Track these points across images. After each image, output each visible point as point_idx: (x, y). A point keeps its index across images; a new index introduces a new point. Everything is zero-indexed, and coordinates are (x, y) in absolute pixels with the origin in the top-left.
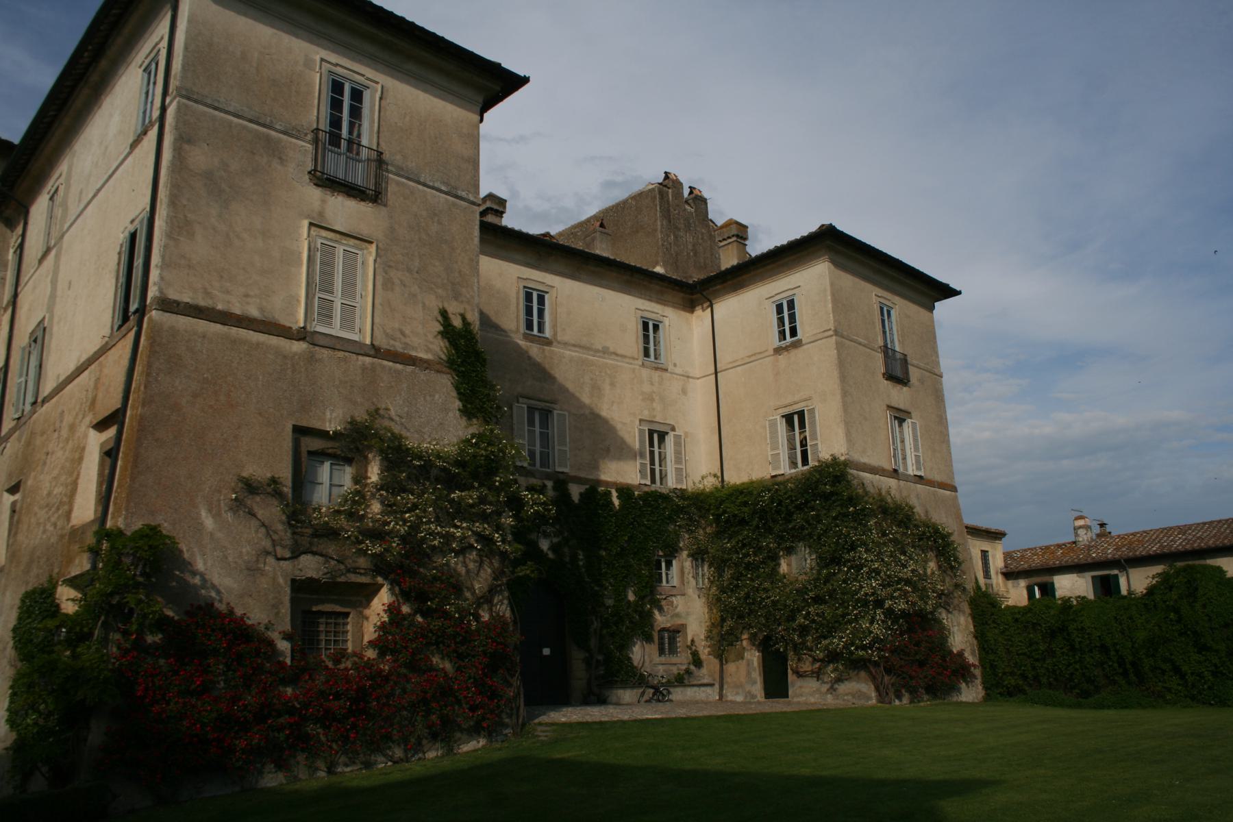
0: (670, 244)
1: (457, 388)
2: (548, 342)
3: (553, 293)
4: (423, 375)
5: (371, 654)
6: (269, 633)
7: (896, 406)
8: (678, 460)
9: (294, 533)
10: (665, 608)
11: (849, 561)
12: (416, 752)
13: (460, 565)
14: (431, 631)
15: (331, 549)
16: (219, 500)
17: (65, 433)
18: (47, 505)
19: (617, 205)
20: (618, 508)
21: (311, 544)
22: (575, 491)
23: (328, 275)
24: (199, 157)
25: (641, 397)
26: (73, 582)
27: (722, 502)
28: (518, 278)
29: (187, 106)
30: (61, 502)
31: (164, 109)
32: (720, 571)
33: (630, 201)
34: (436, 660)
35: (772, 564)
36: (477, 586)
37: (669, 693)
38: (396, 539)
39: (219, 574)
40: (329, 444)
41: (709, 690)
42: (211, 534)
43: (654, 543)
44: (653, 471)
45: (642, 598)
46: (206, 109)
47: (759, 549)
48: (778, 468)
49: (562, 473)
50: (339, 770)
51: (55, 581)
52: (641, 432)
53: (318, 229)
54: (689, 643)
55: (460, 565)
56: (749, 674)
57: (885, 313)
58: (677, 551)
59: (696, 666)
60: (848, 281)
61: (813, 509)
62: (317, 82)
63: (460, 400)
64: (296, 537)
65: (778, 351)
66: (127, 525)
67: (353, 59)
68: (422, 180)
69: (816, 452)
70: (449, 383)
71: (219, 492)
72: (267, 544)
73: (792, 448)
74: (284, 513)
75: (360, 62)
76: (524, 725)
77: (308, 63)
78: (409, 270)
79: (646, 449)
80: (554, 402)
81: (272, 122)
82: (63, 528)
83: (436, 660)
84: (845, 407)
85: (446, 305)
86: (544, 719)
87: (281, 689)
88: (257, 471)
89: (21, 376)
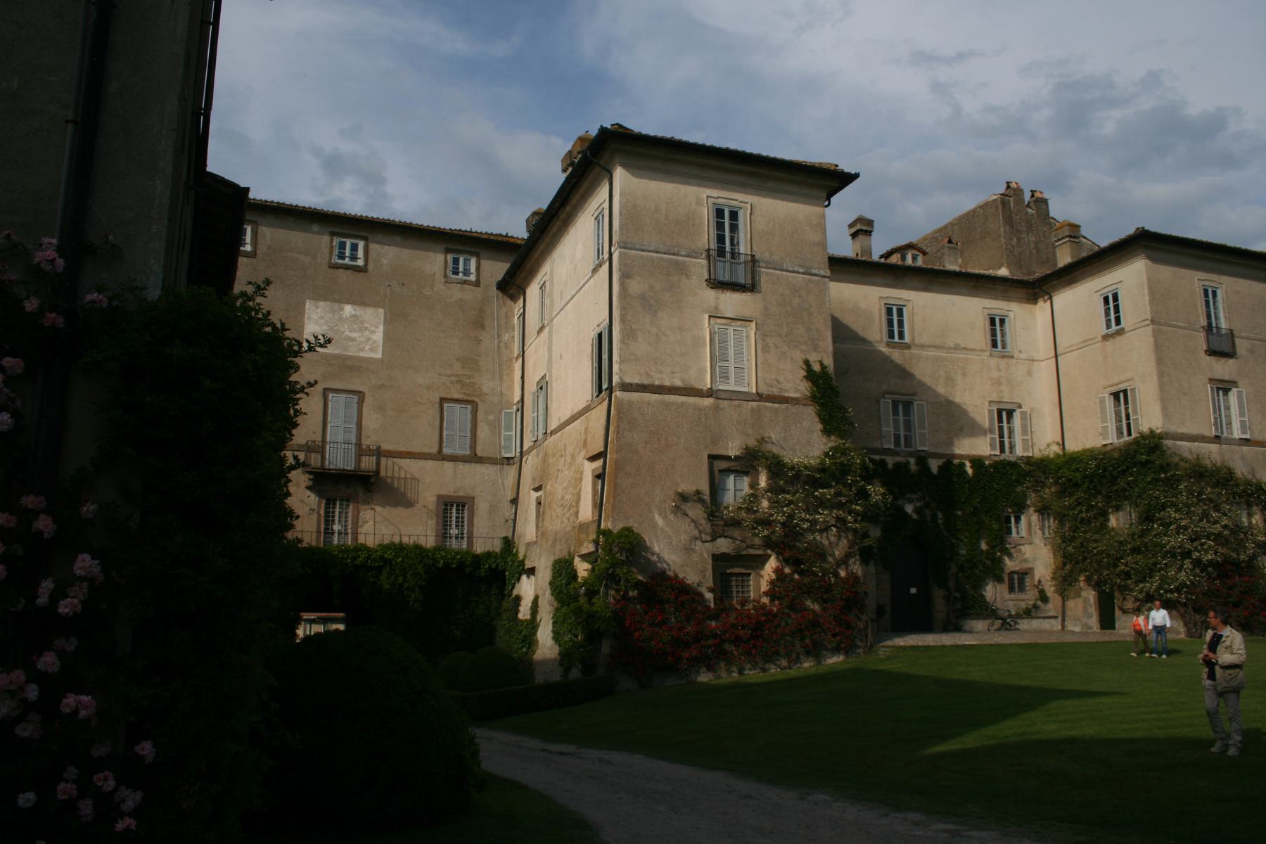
0: (1013, 246)
1: (819, 415)
2: (908, 347)
3: (910, 306)
4: (794, 409)
5: (765, 600)
6: (700, 588)
7: (1221, 378)
8: (1024, 432)
9: (712, 525)
10: (1015, 555)
11: (1160, 519)
12: (796, 664)
13: (824, 539)
14: (804, 584)
15: (737, 533)
16: (665, 508)
17: (568, 459)
18: (562, 506)
19: (969, 213)
20: (971, 475)
21: (723, 531)
22: (934, 465)
23: (724, 349)
24: (635, 286)
25: (989, 383)
26: (584, 557)
27: (1060, 469)
28: (880, 297)
29: (625, 253)
30: (571, 505)
31: (611, 255)
32: (1061, 523)
33: (978, 210)
34: (809, 603)
35: (1101, 519)
36: (837, 553)
37: (1016, 623)
38: (778, 525)
39: (668, 553)
40: (732, 464)
41: (1053, 621)
42: (662, 529)
43: (1003, 502)
44: (1002, 444)
45: (993, 547)
46: (636, 252)
47: (1090, 508)
48: (1108, 438)
49: (923, 451)
50: (746, 672)
51: (572, 556)
52: (990, 412)
53: (714, 319)
54: (1036, 583)
55: (824, 539)
56: (1085, 610)
57: (1209, 295)
58: (1024, 508)
59: (1042, 602)
60: (1167, 273)
61: (1132, 475)
62: (705, 215)
63: (822, 423)
64: (714, 527)
65: (1106, 337)
66: (614, 527)
67: (729, 190)
68: (785, 268)
69: (1137, 425)
70: (813, 412)
71: (665, 502)
72: (696, 533)
73: (1118, 419)
74: (705, 512)
75: (734, 191)
76: (871, 647)
77: (699, 203)
78: (780, 336)
79: (995, 425)
80: (914, 394)
81: (678, 250)
82: (574, 522)
83: (809, 603)
84: (1162, 386)
85: (808, 357)
86: (889, 643)
87: (709, 622)
88: (686, 487)
89: (534, 412)
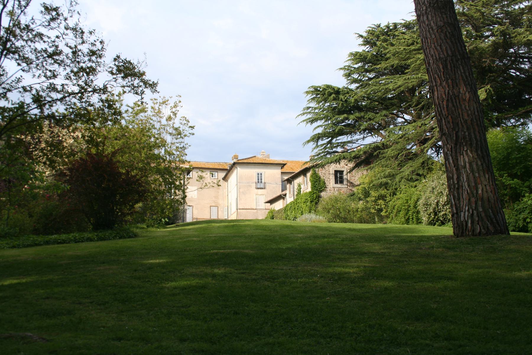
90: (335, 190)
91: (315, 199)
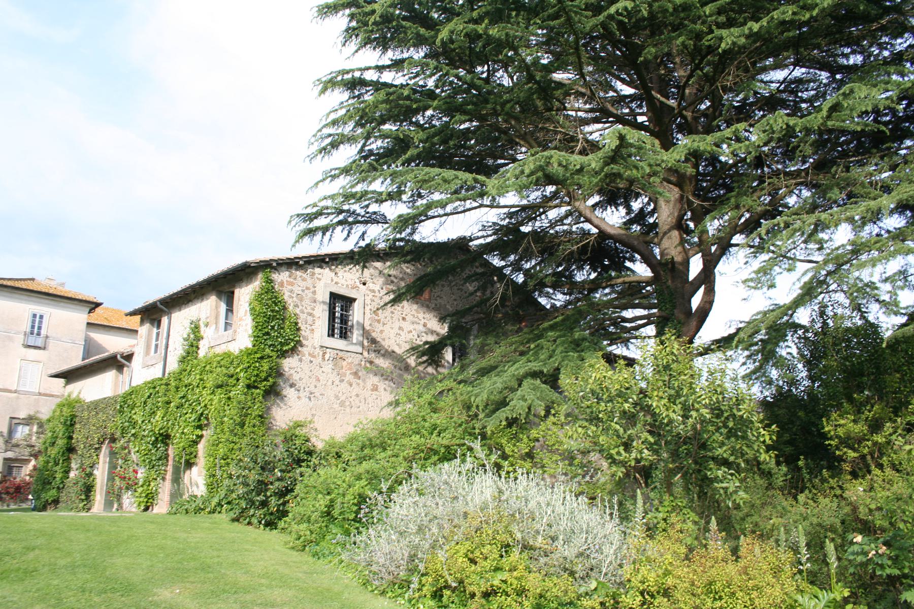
5: (28, 478)
90: (327, 357)
91: (266, 379)
